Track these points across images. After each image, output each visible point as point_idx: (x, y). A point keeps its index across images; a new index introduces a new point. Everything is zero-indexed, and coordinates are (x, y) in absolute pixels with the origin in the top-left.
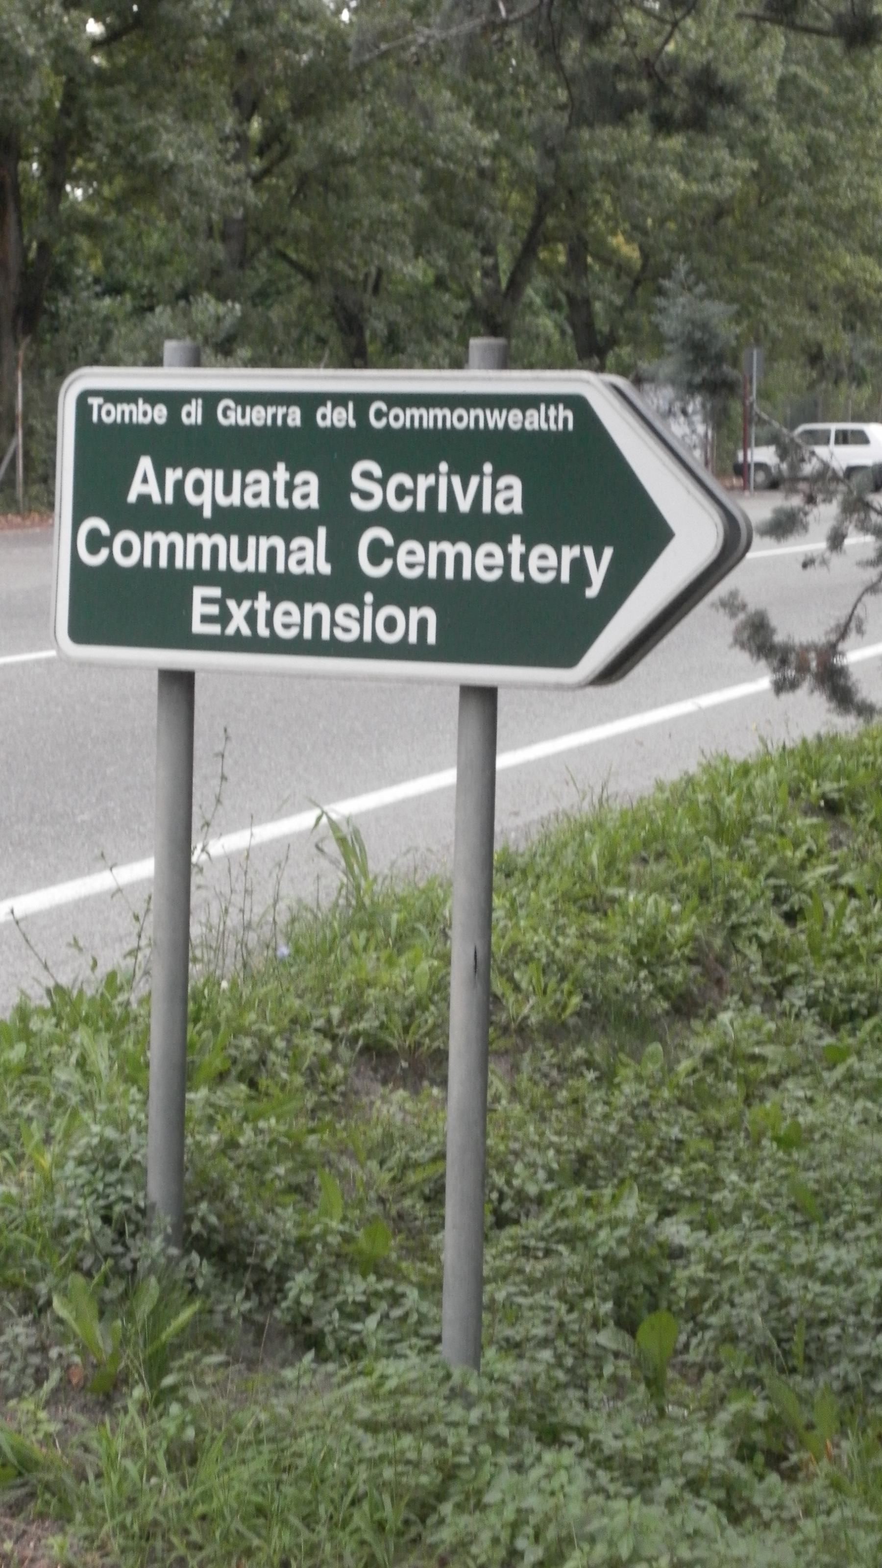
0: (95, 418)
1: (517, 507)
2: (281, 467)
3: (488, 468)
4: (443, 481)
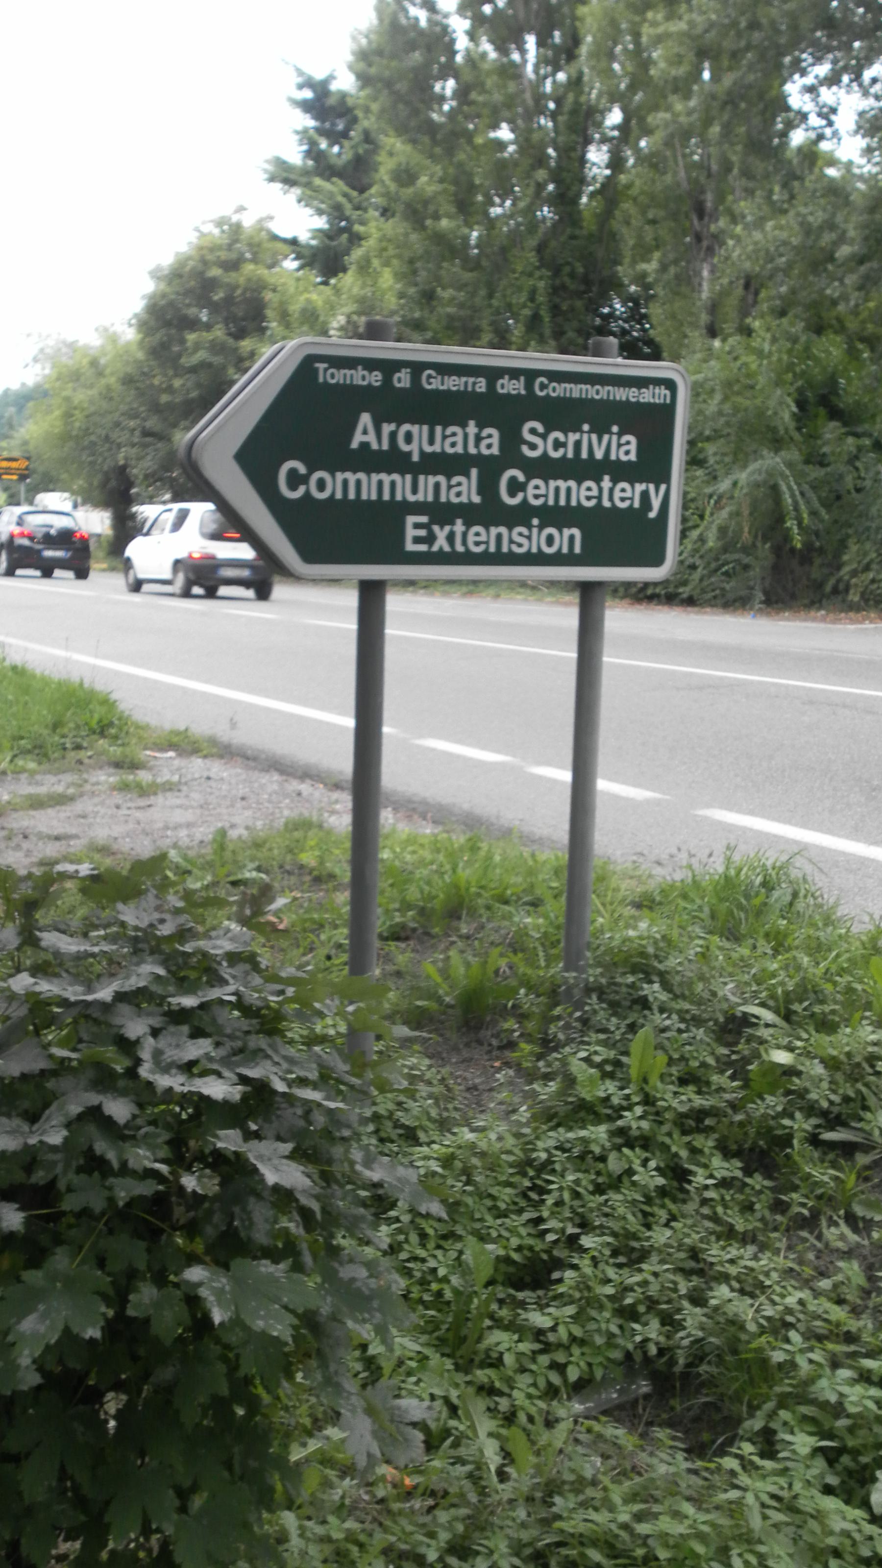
0: (321, 380)
1: (633, 457)
2: (472, 423)
3: (615, 429)
4: (585, 436)
